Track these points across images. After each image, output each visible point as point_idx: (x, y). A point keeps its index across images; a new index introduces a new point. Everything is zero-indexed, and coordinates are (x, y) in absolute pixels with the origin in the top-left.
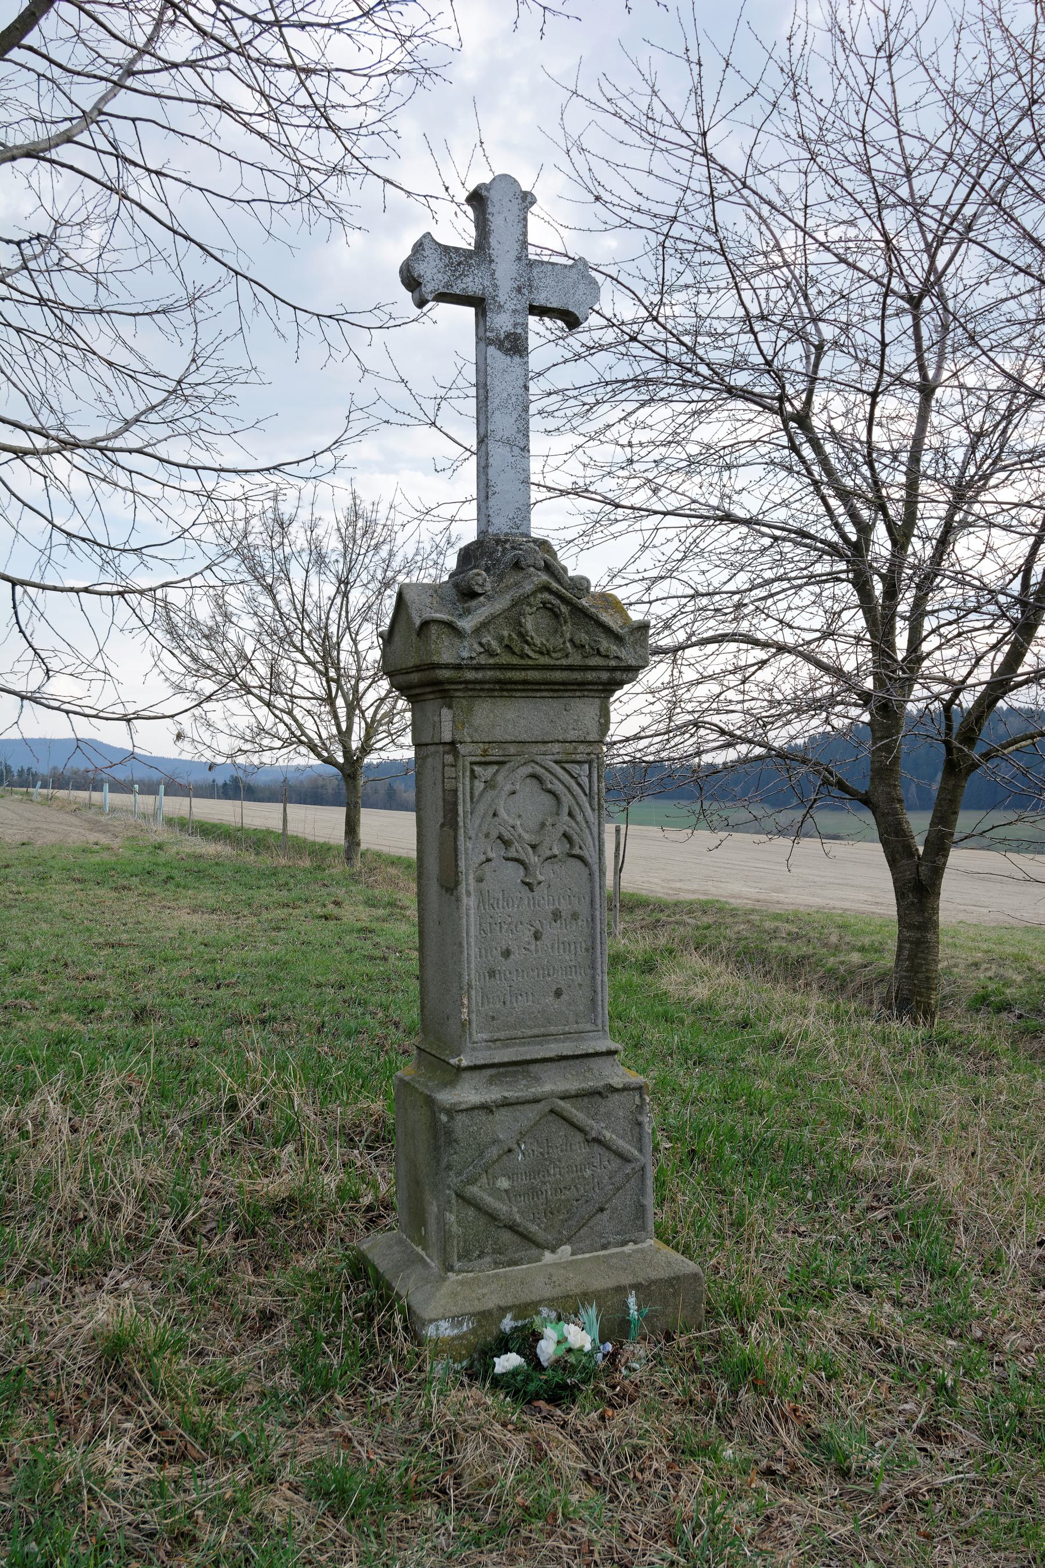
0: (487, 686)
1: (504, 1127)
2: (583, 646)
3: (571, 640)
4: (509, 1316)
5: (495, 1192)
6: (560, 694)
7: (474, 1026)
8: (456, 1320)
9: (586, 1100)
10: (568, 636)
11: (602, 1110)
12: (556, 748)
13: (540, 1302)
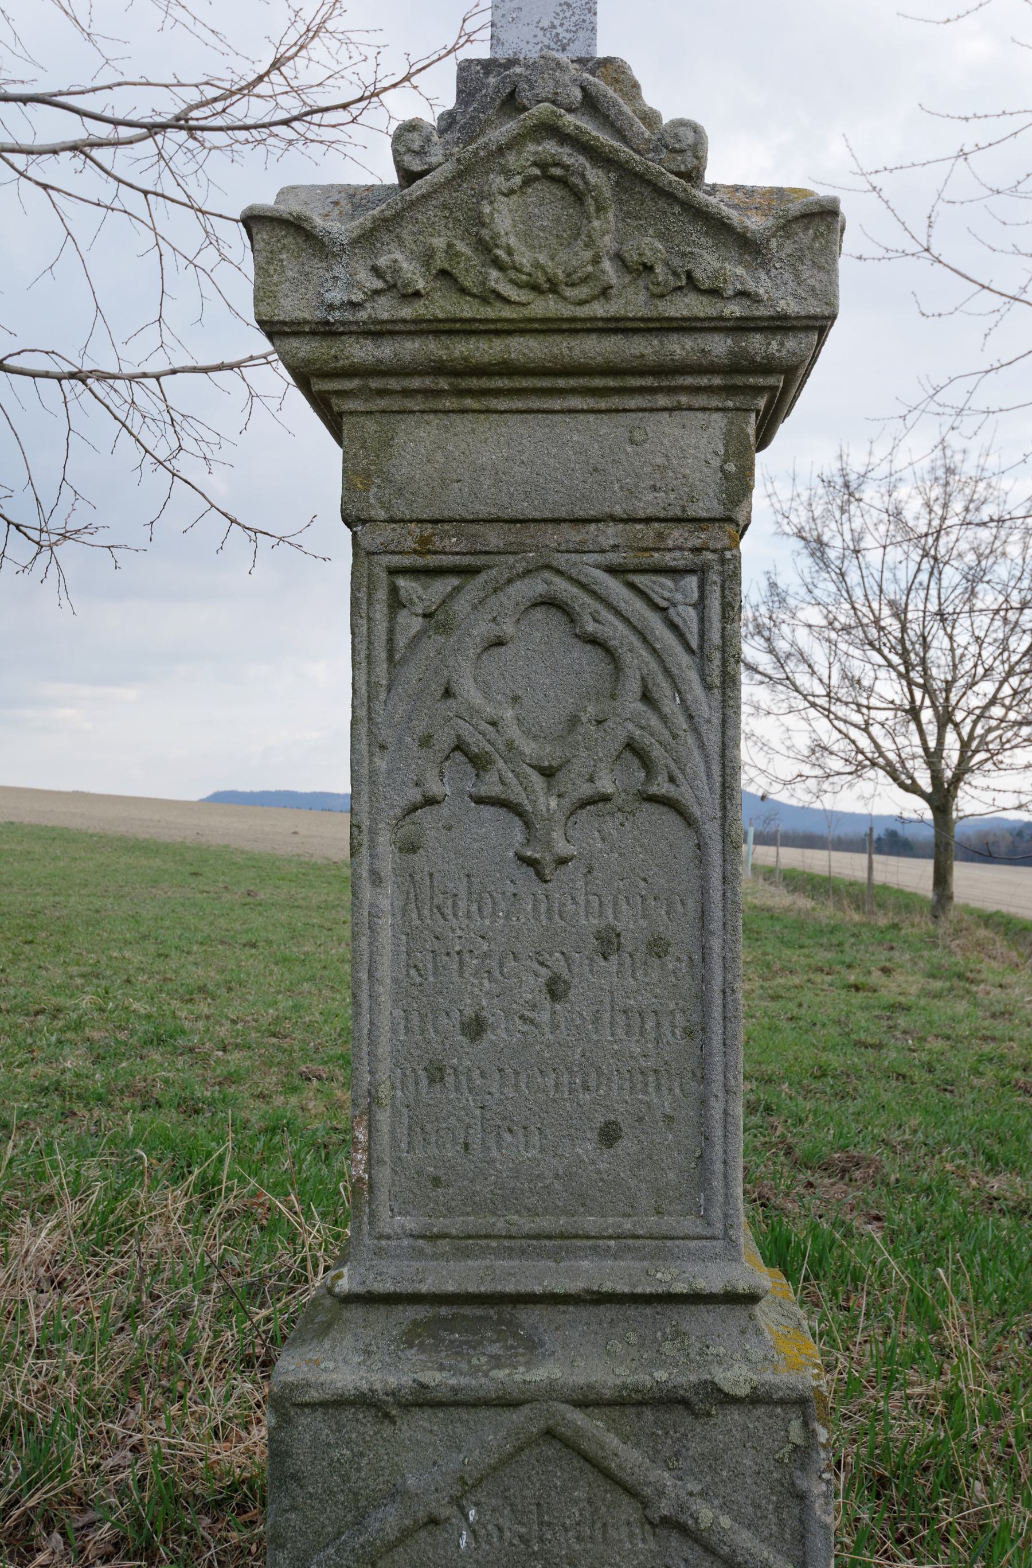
0: (416, 383)
1: (423, 1460)
2: (649, 268)
3: (618, 257)
6: (615, 402)
7: (383, 1195)
9: (648, 1414)
10: (608, 243)
11: (695, 1447)
12: (610, 534)
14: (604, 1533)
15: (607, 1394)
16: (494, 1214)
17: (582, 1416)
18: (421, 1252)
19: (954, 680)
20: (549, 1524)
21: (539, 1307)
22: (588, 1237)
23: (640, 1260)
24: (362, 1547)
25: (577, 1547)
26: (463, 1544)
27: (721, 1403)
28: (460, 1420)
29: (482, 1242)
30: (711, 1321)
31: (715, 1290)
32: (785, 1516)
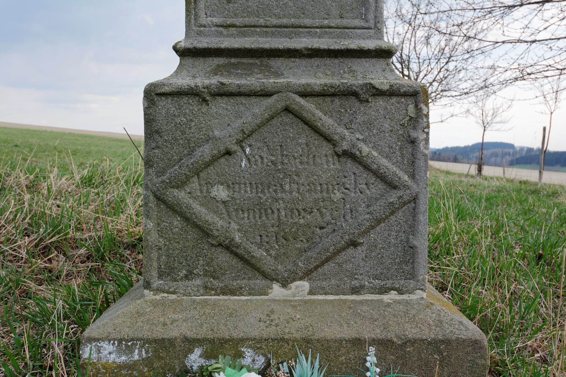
4: (198, 352)
5: (210, 202)
8: (124, 344)
9: (337, 101)
11: (360, 118)
13: (242, 341)
14: (314, 160)
15: (317, 89)
16: (258, 17)
17: (303, 101)
18: (221, 33)
19: (420, 72)
20: (287, 155)
21: (281, 59)
22: (306, 27)
23: (332, 38)
24: (192, 164)
25: (300, 167)
26: (243, 165)
27: (374, 95)
28: (241, 103)
29: (252, 29)
30: (367, 66)
31: (371, 48)
32: (404, 152)
